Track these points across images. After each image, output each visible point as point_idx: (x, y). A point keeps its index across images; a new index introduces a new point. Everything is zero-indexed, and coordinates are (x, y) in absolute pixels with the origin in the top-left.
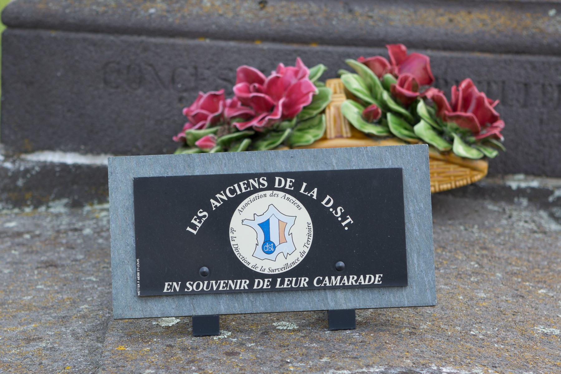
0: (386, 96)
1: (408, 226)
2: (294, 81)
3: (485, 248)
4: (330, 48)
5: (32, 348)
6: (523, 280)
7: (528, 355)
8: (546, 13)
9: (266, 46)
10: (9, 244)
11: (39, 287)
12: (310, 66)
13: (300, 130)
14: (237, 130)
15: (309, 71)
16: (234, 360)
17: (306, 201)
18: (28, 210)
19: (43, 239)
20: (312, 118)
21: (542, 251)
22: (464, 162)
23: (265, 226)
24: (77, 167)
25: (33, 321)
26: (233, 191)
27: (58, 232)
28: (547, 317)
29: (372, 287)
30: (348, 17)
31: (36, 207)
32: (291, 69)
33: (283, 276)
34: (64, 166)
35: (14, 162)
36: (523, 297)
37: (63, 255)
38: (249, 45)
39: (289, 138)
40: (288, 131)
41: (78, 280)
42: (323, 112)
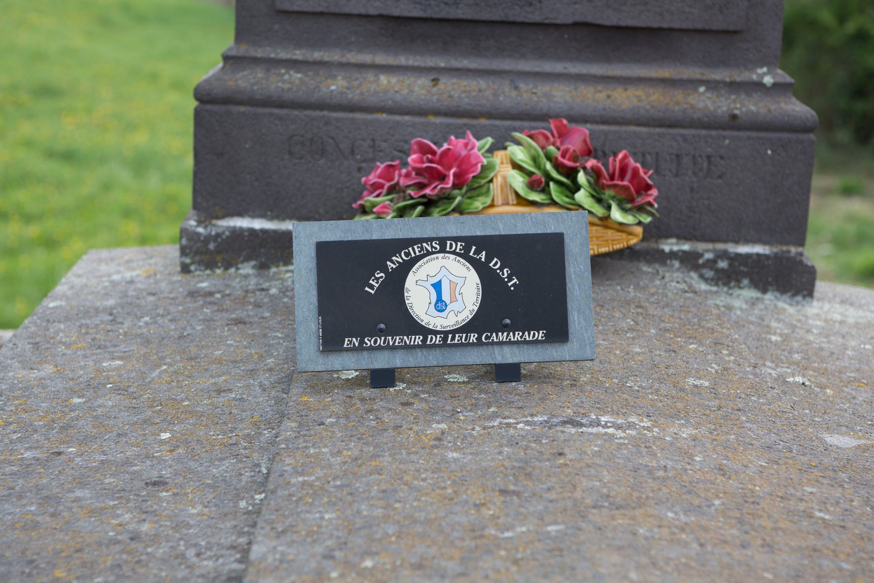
0: (548, 166)
1: (569, 286)
2: (464, 153)
5: (222, 399)
6: (676, 336)
9: (438, 120)
10: (201, 302)
12: (478, 139)
13: (469, 198)
14: (412, 198)
15: (478, 144)
16: (409, 410)
18: (218, 271)
19: (232, 298)
20: (481, 187)
21: (693, 309)
22: (621, 227)
23: (437, 286)
24: (264, 232)
27: (247, 291)
28: (697, 370)
29: (536, 342)
30: (514, 93)
31: (226, 268)
32: (461, 141)
33: (454, 332)
34: (252, 231)
35: (205, 227)
38: (422, 120)
40: (458, 199)
41: (265, 336)
42: (491, 181)
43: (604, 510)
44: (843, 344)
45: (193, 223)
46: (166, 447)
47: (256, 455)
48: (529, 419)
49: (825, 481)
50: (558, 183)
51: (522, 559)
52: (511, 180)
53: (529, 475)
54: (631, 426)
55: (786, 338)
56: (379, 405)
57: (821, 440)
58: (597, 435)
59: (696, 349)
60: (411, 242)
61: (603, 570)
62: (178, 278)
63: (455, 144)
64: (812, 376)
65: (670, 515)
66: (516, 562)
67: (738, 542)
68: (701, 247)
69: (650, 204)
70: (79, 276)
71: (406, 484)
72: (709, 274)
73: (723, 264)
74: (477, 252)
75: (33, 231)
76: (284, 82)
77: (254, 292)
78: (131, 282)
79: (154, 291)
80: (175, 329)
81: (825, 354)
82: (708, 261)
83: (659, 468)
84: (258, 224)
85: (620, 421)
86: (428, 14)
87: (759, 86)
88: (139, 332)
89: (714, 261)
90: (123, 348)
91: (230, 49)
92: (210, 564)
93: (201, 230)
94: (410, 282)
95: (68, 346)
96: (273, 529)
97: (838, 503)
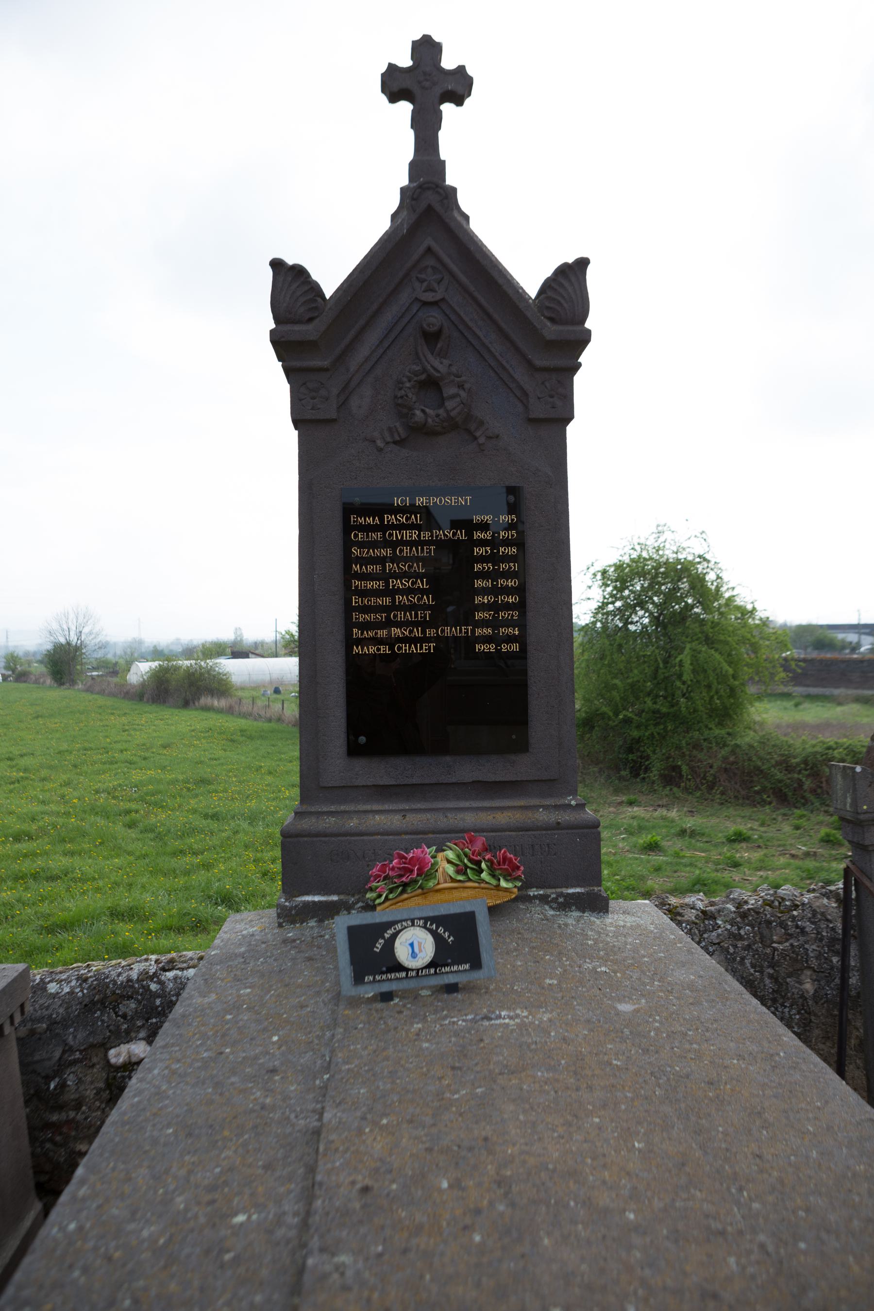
0: (466, 861)
1: (480, 939)
2: (422, 856)
3: (520, 933)
4: (438, 836)
5: (304, 1012)
6: (539, 952)
7: (542, 999)
8: (538, 810)
9: (407, 837)
10: (289, 947)
11: (306, 973)
12: (428, 848)
13: (426, 880)
14: (396, 883)
15: (428, 851)
16: (402, 1016)
17: (430, 931)
18: (297, 925)
19: (306, 943)
20: (431, 874)
21: (547, 932)
22: (506, 890)
23: (412, 945)
24: (320, 902)
25: (303, 995)
26: (395, 929)
27: (313, 938)
28: (551, 973)
29: (465, 970)
30: (445, 820)
31: (302, 924)
32: (420, 850)
33: (422, 969)
34: (314, 902)
35: (290, 902)
36: (538, 962)
37: (316, 953)
38: (399, 837)
39: (421, 884)
40: (420, 882)
41: (324, 968)
42: (437, 871)
43: (505, 1076)
44: (625, 942)
45: (283, 900)
46: (276, 1046)
47: (323, 1049)
48: (464, 1017)
49: (618, 1040)
50: (472, 869)
51: (464, 1112)
52: (447, 870)
53: (465, 1056)
54: (517, 1016)
55: (596, 942)
56: (386, 1013)
57: (615, 1008)
58: (500, 1025)
59: (549, 959)
60: (396, 922)
61: (506, 1116)
62: (276, 931)
64: (609, 965)
65: (539, 1074)
66: (461, 1115)
67: (574, 1088)
68: (549, 891)
69: (520, 876)
70: (226, 933)
71: (402, 1066)
72: (555, 905)
73: (561, 900)
74: (431, 925)
75: (198, 860)
76: (326, 823)
77: (316, 938)
78: (253, 935)
79: (265, 940)
80: (277, 966)
81: (616, 949)
82: (553, 898)
83: (532, 1043)
84: (317, 898)
85: (512, 1014)
86: (398, 782)
87: (570, 805)
88: (258, 969)
89: (557, 898)
90: (250, 980)
91: (298, 808)
92: (302, 1122)
93: (287, 904)
95: (222, 980)
96: (334, 1101)
97: (624, 1053)
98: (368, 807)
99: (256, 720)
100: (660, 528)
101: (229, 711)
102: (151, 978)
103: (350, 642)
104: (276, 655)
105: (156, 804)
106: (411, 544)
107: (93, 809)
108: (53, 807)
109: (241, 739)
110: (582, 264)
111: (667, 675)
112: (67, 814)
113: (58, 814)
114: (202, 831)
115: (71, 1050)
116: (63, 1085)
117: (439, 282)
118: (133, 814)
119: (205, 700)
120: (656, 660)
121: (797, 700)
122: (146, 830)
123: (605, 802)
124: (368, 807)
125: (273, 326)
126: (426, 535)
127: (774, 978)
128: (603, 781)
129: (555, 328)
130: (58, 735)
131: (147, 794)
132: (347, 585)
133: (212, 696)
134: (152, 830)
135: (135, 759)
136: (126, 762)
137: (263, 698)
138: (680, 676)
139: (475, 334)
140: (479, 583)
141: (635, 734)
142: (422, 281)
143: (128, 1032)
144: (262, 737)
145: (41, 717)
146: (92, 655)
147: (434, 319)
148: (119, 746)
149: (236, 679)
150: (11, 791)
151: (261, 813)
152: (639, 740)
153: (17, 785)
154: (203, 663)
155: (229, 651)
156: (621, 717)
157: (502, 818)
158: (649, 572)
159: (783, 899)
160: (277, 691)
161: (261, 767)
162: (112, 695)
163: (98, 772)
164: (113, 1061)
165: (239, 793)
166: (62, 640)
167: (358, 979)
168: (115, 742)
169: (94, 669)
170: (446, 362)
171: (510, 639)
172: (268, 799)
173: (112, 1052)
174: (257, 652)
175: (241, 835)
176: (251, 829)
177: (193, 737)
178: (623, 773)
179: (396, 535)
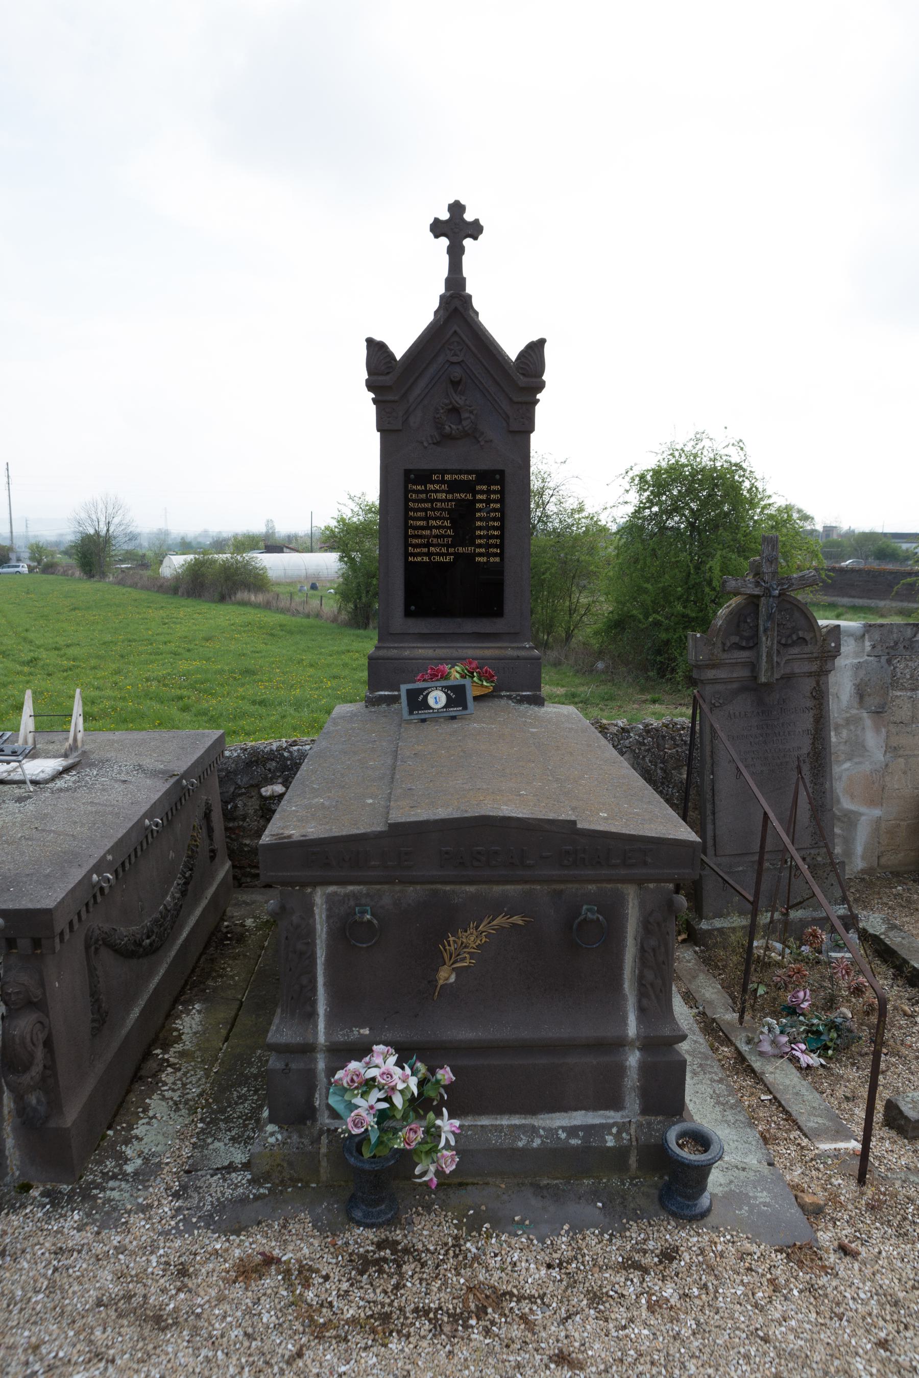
63: (441, 667)
84: (386, 693)
87: (525, 647)
94: (429, 697)
98: (415, 645)
99: (294, 615)
100: (698, 436)
101: (267, 606)
102: (284, 749)
103: (407, 554)
104: (311, 550)
105: (205, 691)
106: (441, 501)
107: (146, 695)
108: (109, 692)
109: (281, 633)
110: (541, 342)
111: (697, 581)
112: (123, 699)
113: (115, 699)
114: (252, 715)
115: (240, 787)
116: (236, 807)
117: (461, 350)
118: (186, 700)
119: (241, 595)
120: (688, 566)
121: (840, 610)
122: (198, 714)
123: (630, 700)
124: (415, 645)
125: (372, 395)
126: (450, 496)
127: (664, 770)
128: (631, 680)
129: (526, 380)
130: (99, 627)
131: (196, 682)
132: (406, 523)
133: (249, 591)
134: (205, 714)
135: (180, 650)
136: (171, 653)
137: (300, 594)
138: (710, 583)
139: (481, 382)
140: (478, 524)
141: (664, 636)
142: (451, 350)
143: (272, 779)
144: (301, 632)
145: (78, 609)
146: (121, 546)
147: (457, 373)
148: (162, 638)
149: (272, 574)
150: (65, 678)
151: (306, 701)
152: (667, 642)
153: (70, 673)
154: (239, 557)
155: (262, 544)
156: (651, 620)
157: (488, 653)
158: (685, 478)
159: (676, 724)
160: (314, 587)
161: (302, 660)
162: (146, 588)
163: (146, 662)
164: (264, 794)
165: (283, 683)
166: (91, 531)
167: (411, 713)
168: (157, 634)
169: (122, 561)
170: (463, 398)
171: (495, 555)
172: (312, 689)
173: (263, 790)
174: (290, 546)
175: (289, 719)
176: (297, 714)
177: (233, 630)
178: (651, 674)
179: (433, 496)
